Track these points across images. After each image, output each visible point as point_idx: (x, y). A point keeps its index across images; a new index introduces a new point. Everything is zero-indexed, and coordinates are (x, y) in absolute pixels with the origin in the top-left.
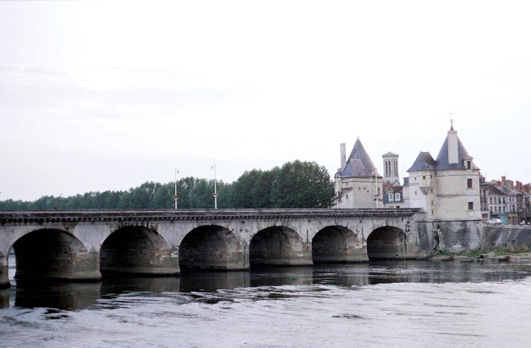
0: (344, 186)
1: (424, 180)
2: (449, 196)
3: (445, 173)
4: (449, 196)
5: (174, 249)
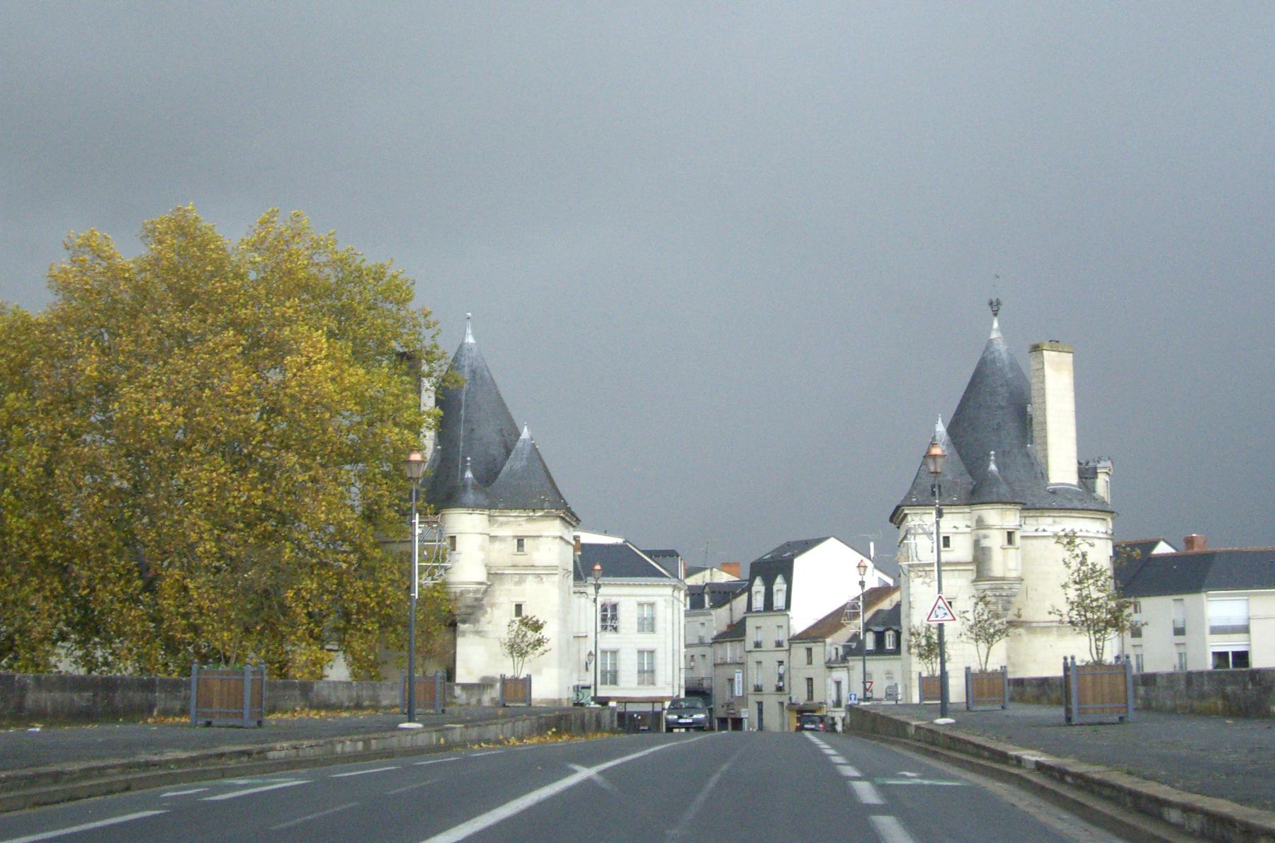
0: (504, 553)
1: (1011, 552)
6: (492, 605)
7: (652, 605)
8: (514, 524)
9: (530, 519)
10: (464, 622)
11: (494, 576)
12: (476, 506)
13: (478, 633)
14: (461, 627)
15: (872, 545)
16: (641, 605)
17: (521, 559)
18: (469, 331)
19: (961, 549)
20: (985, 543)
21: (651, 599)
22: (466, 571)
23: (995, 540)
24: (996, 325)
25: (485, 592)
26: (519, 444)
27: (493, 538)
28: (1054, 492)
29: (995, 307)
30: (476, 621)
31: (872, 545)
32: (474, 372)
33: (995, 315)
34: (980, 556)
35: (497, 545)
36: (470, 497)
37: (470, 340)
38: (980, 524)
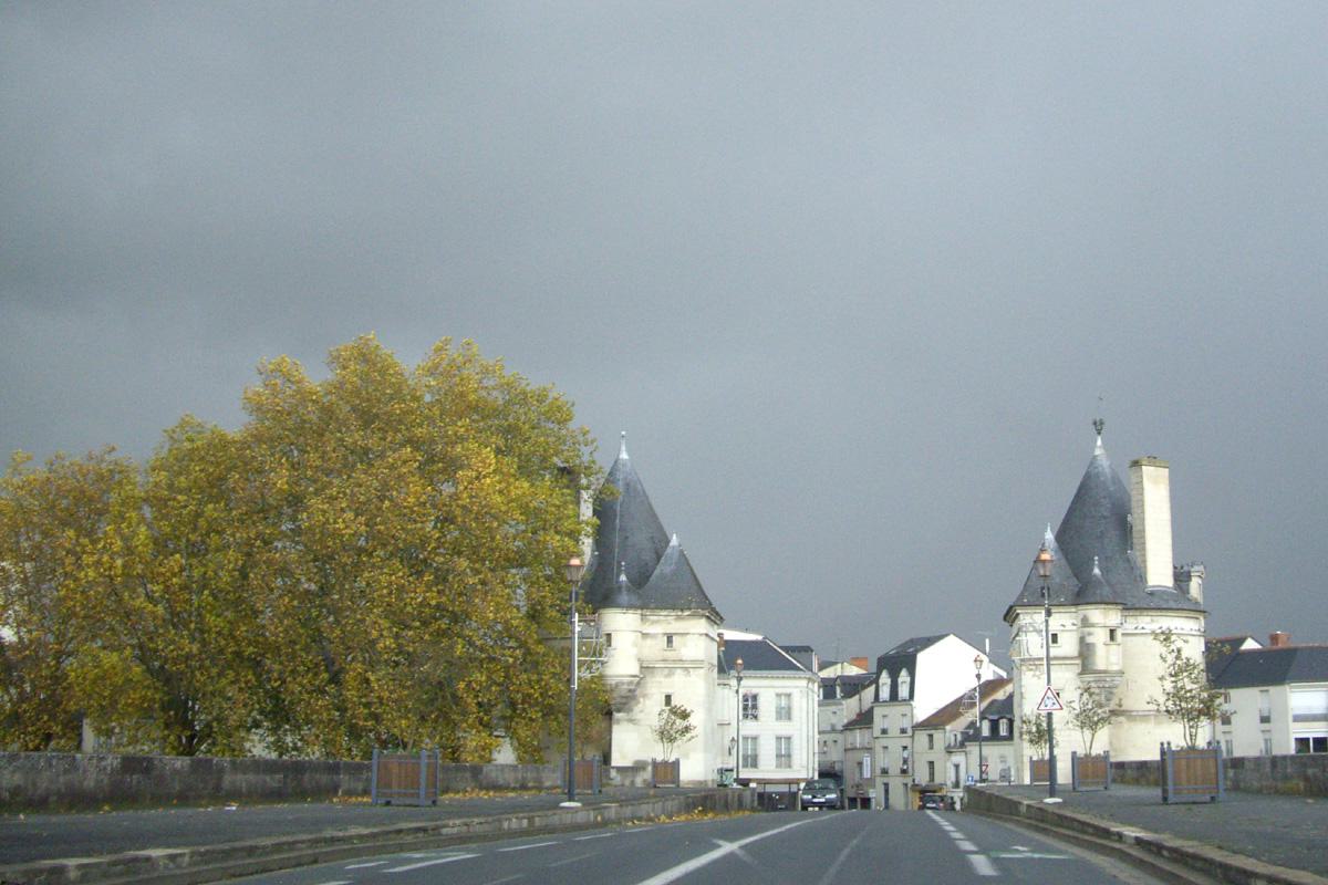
0: (654, 649)
1: (1114, 648)
6: (644, 696)
7: (789, 695)
8: (664, 622)
9: (679, 618)
10: (619, 711)
11: (646, 669)
12: (630, 607)
13: (631, 721)
14: (617, 715)
15: (987, 641)
16: (778, 695)
17: (670, 655)
18: (623, 448)
19: (1068, 645)
20: (1089, 640)
21: (788, 691)
22: (621, 664)
23: (1099, 637)
24: (1099, 443)
25: (638, 683)
26: (669, 550)
27: (645, 635)
28: (1152, 594)
29: (1098, 426)
30: (630, 710)
31: (987, 641)
32: (628, 485)
33: (1099, 433)
35: (649, 642)
36: (624, 598)
37: (624, 456)
38: (1085, 622)
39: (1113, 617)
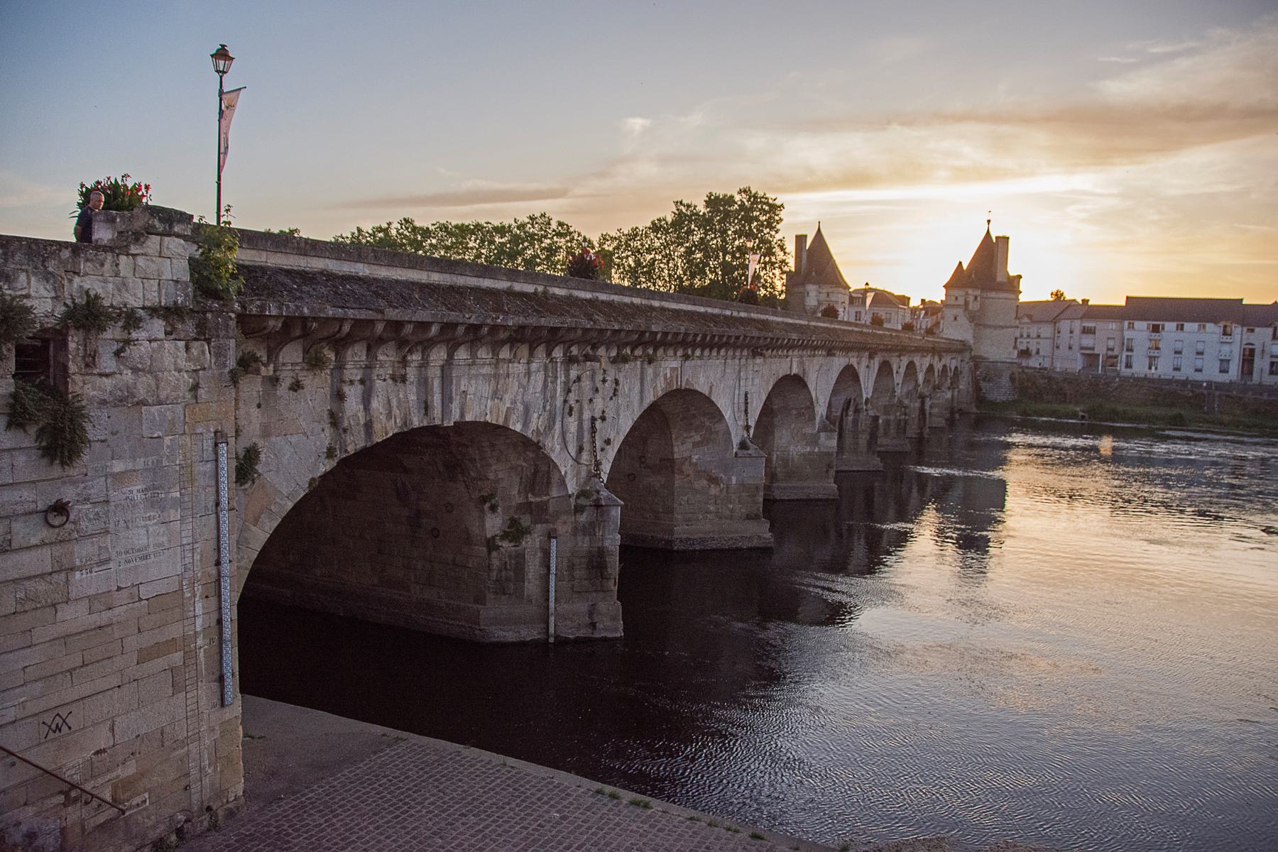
2: (996, 327)
3: (993, 294)
4: (996, 327)
5: (824, 429)
19: (961, 301)
23: (971, 299)
34: (966, 303)
39: (978, 293)
